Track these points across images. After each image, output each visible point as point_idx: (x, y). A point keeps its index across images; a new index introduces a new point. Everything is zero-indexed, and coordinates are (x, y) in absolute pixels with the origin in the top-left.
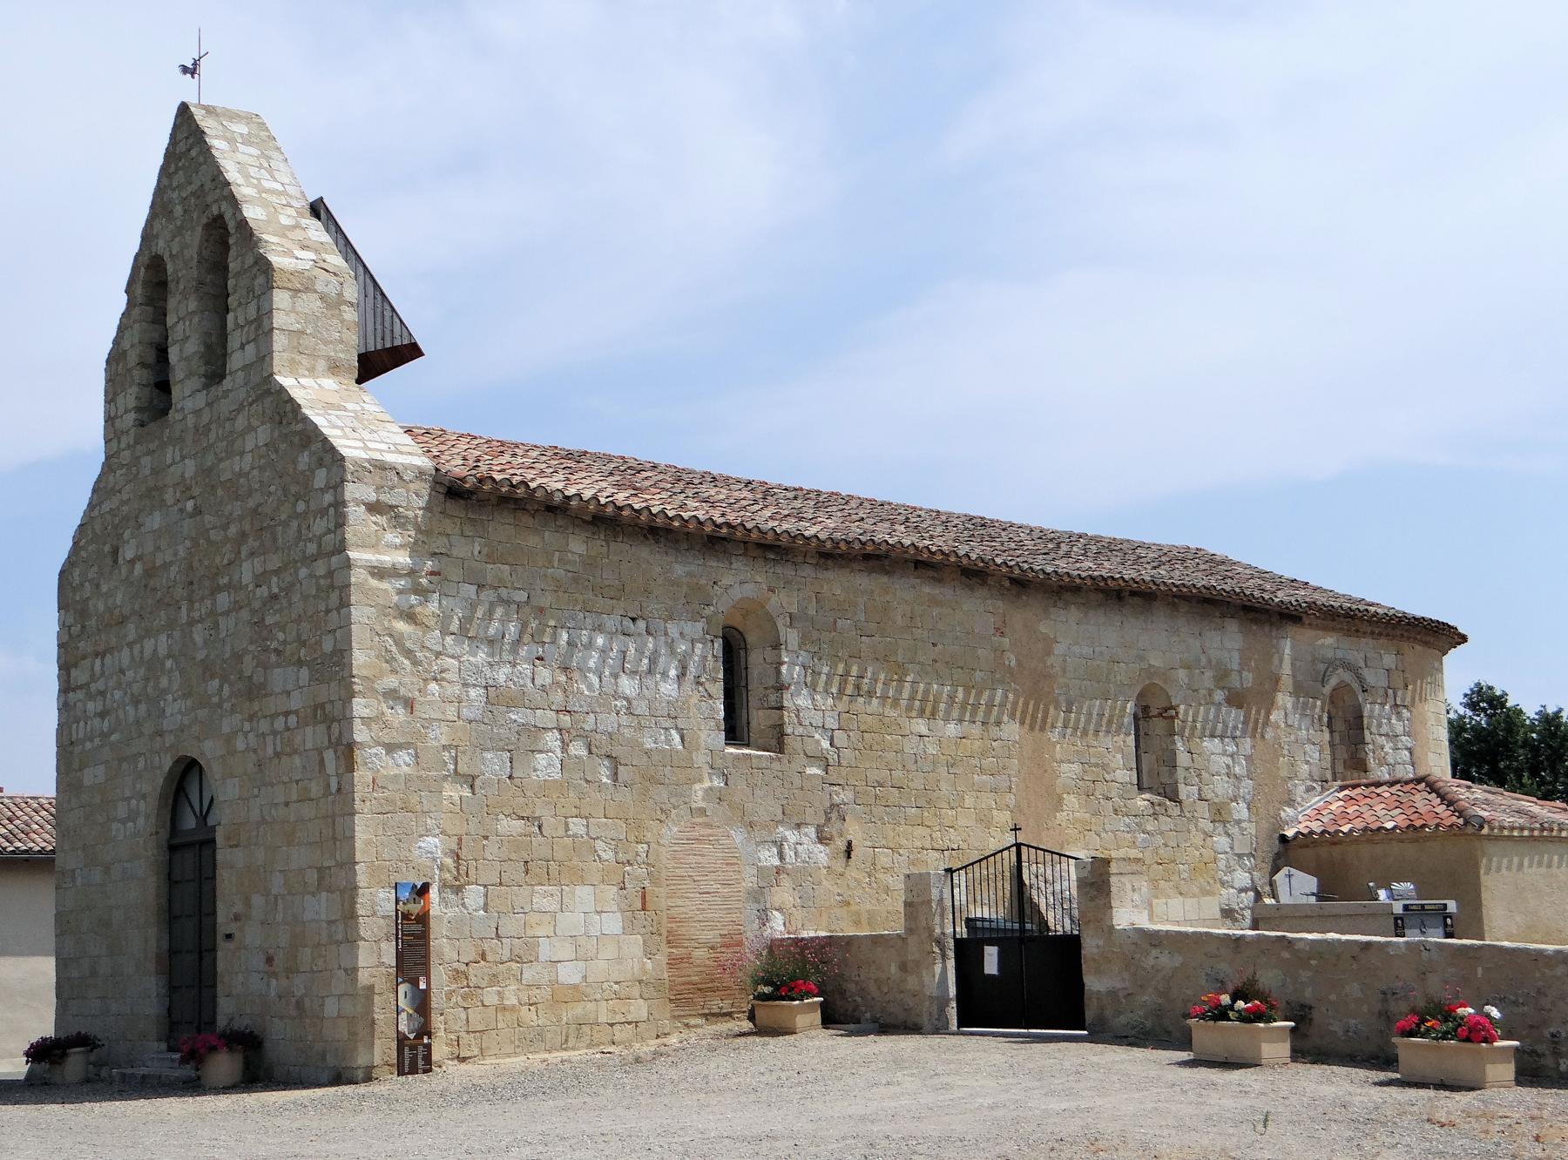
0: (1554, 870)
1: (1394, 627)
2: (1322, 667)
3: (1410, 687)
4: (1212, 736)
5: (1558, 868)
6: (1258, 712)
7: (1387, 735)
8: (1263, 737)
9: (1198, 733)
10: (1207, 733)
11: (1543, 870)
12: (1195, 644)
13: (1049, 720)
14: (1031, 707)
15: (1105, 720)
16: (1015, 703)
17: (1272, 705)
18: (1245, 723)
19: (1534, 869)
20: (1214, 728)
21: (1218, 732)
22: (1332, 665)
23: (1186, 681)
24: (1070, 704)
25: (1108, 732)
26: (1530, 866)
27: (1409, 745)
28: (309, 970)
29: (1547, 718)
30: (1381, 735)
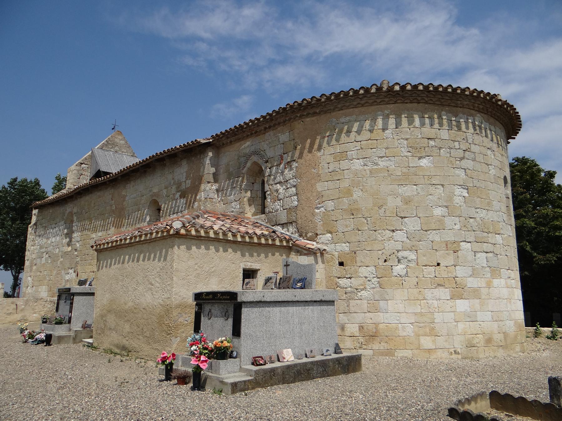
0: (126, 265)
1: (306, 108)
2: (242, 159)
3: (299, 147)
4: (174, 214)
5: (128, 263)
6: (191, 197)
7: (280, 183)
8: (193, 207)
9: (168, 214)
10: (172, 213)
11: (120, 265)
12: (170, 177)
13: (123, 224)
14: (116, 220)
15: (138, 218)
16: (114, 221)
17: (198, 191)
18: (186, 204)
19: (116, 266)
20: (174, 210)
21: (176, 211)
22: (248, 157)
23: (166, 193)
24: (129, 216)
25: (138, 223)
26: (143, 260)
27: (295, 184)
28: (407, 299)
29: (331, 131)
30: (276, 184)
